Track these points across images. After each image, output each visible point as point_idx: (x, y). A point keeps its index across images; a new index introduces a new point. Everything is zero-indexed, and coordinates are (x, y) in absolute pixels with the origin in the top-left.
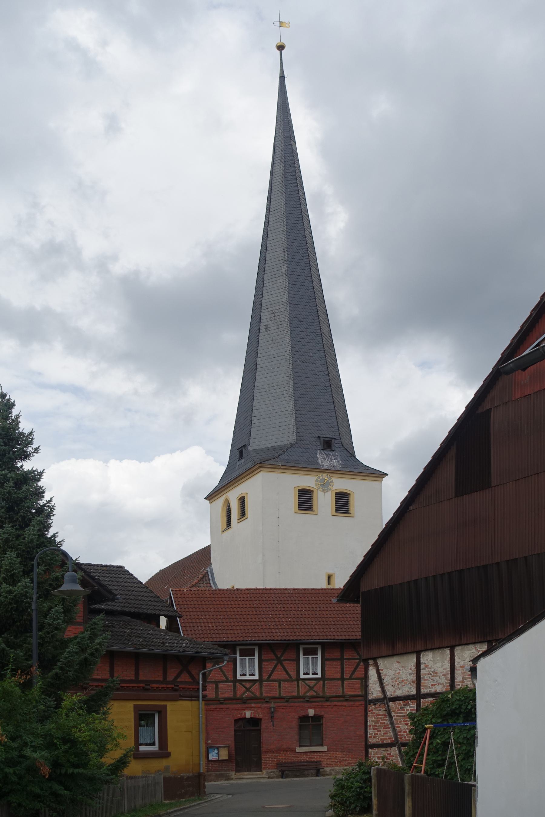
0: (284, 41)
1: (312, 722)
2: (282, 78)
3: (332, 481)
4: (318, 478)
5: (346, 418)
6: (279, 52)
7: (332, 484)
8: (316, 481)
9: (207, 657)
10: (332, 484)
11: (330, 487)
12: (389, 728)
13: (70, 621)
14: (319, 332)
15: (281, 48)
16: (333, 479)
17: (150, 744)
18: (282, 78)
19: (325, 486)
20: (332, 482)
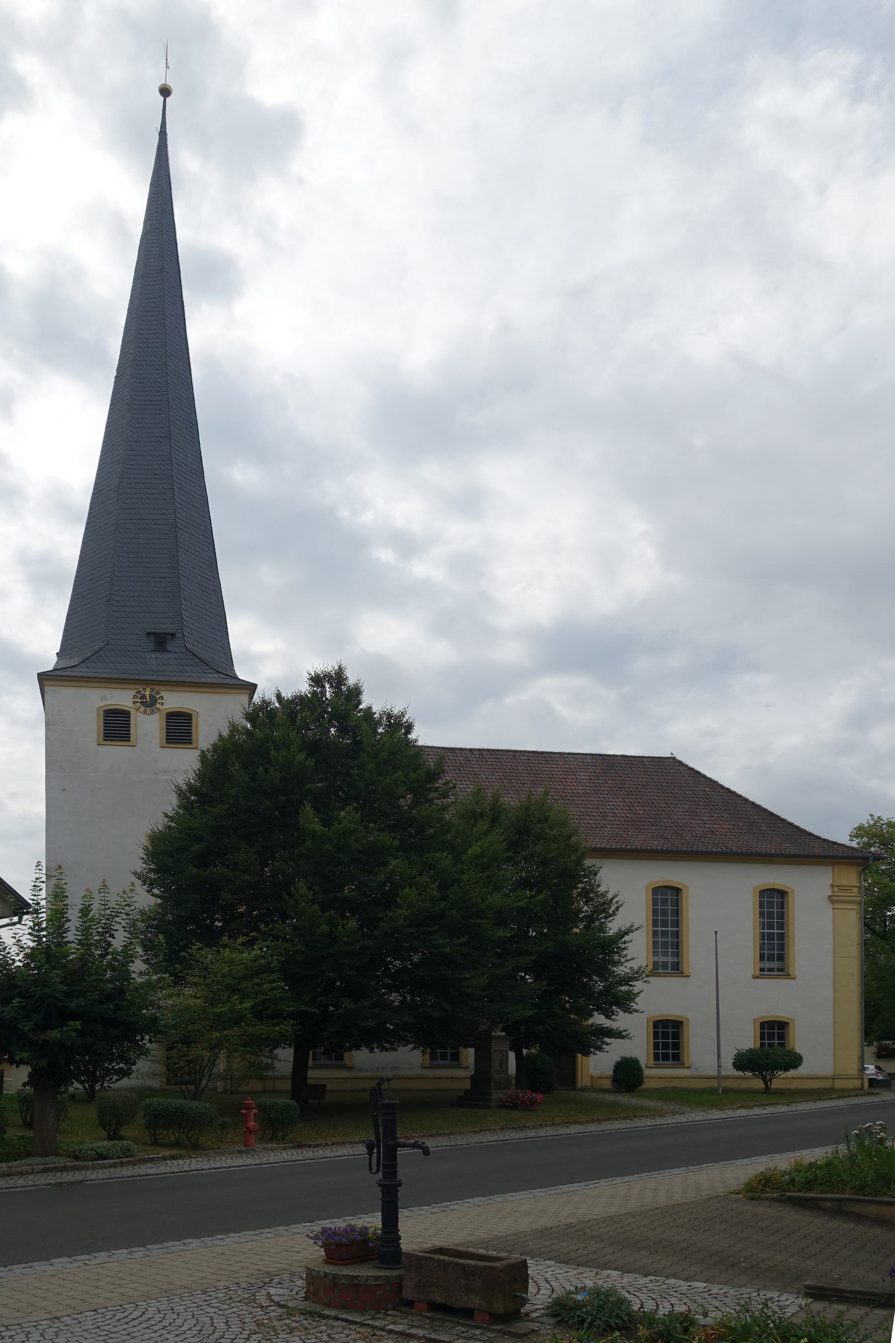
0: (170, 83)
1: (777, 930)
2: (163, 134)
3: (162, 697)
4: (137, 693)
5: (190, 399)
6: (162, 98)
7: (162, 701)
8: (134, 697)
9: (774, 1199)
10: (162, 701)
11: (158, 705)
12: (43, 882)
13: (853, 1145)
14: (181, 636)
15: (165, 92)
16: (163, 694)
17: (496, 1050)
18: (163, 134)
19: (150, 704)
20: (162, 698)
